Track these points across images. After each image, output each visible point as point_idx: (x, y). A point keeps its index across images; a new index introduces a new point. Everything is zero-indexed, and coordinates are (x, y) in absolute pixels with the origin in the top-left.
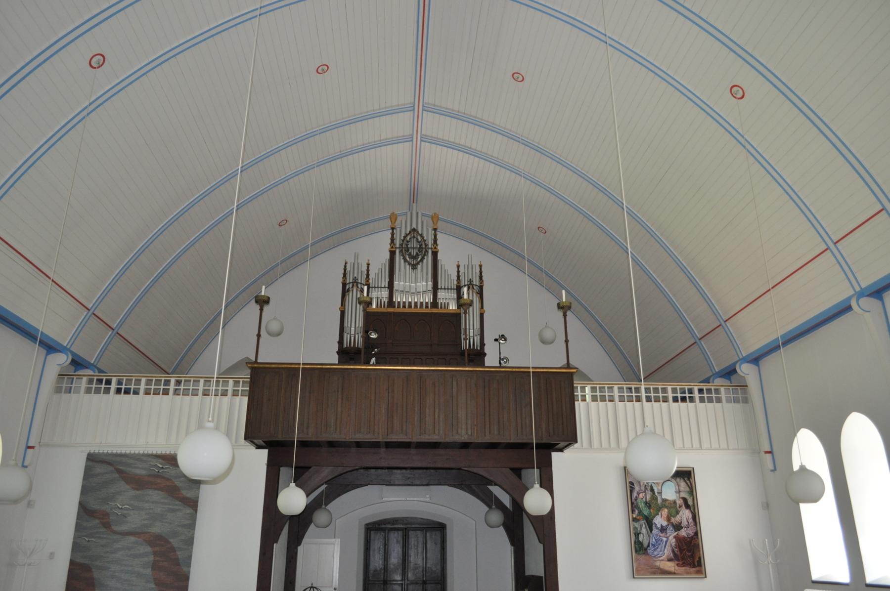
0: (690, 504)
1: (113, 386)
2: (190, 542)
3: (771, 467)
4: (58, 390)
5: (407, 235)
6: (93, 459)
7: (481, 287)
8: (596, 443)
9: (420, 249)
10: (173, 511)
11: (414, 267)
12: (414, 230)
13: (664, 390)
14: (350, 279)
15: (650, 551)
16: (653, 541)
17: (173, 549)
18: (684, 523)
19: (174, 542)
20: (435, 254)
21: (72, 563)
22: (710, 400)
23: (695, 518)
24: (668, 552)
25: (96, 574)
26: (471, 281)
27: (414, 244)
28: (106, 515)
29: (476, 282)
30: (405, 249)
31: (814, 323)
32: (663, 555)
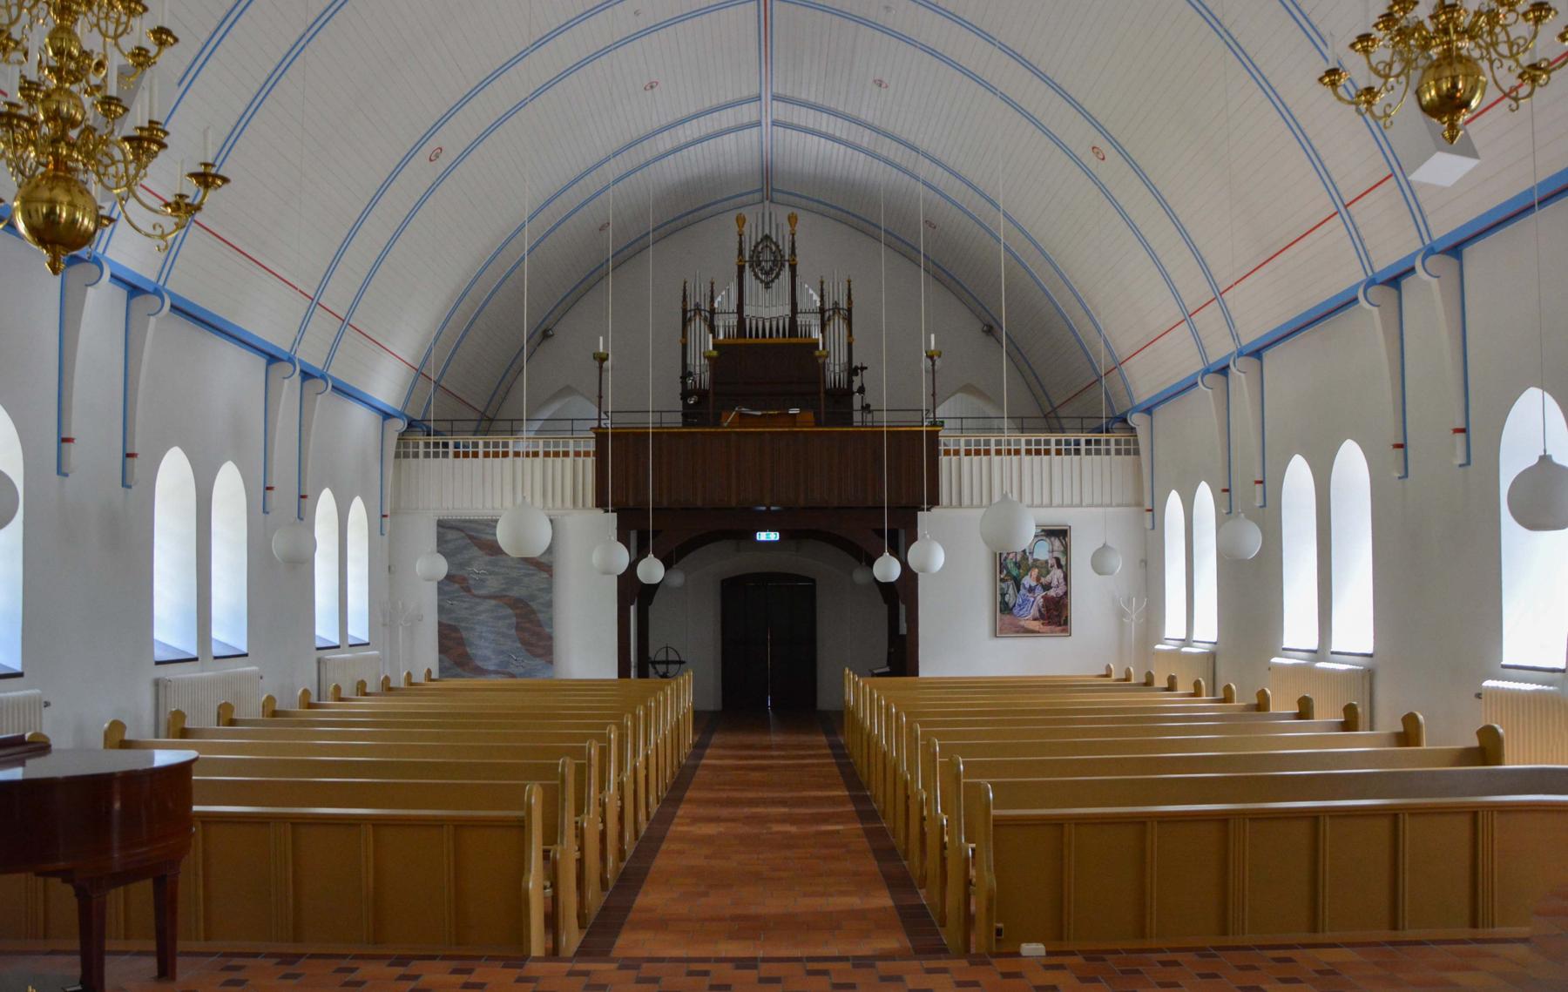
0: (1063, 565)
1: (451, 450)
2: (549, 604)
3: (1461, 459)
4: (397, 456)
6: (442, 525)
7: (849, 310)
8: (966, 500)
9: (775, 262)
10: (526, 575)
11: (767, 285)
12: (767, 238)
13: (1047, 442)
14: (691, 306)
15: (1015, 611)
16: (1020, 601)
17: (533, 612)
18: (1055, 583)
19: (534, 605)
20: (793, 268)
21: (440, 624)
22: (1098, 452)
23: (1066, 578)
24: (1034, 611)
25: (464, 634)
26: (836, 303)
27: (767, 255)
28: (464, 579)
29: (843, 304)
30: (756, 263)
31: (1325, 311)
32: (1028, 617)
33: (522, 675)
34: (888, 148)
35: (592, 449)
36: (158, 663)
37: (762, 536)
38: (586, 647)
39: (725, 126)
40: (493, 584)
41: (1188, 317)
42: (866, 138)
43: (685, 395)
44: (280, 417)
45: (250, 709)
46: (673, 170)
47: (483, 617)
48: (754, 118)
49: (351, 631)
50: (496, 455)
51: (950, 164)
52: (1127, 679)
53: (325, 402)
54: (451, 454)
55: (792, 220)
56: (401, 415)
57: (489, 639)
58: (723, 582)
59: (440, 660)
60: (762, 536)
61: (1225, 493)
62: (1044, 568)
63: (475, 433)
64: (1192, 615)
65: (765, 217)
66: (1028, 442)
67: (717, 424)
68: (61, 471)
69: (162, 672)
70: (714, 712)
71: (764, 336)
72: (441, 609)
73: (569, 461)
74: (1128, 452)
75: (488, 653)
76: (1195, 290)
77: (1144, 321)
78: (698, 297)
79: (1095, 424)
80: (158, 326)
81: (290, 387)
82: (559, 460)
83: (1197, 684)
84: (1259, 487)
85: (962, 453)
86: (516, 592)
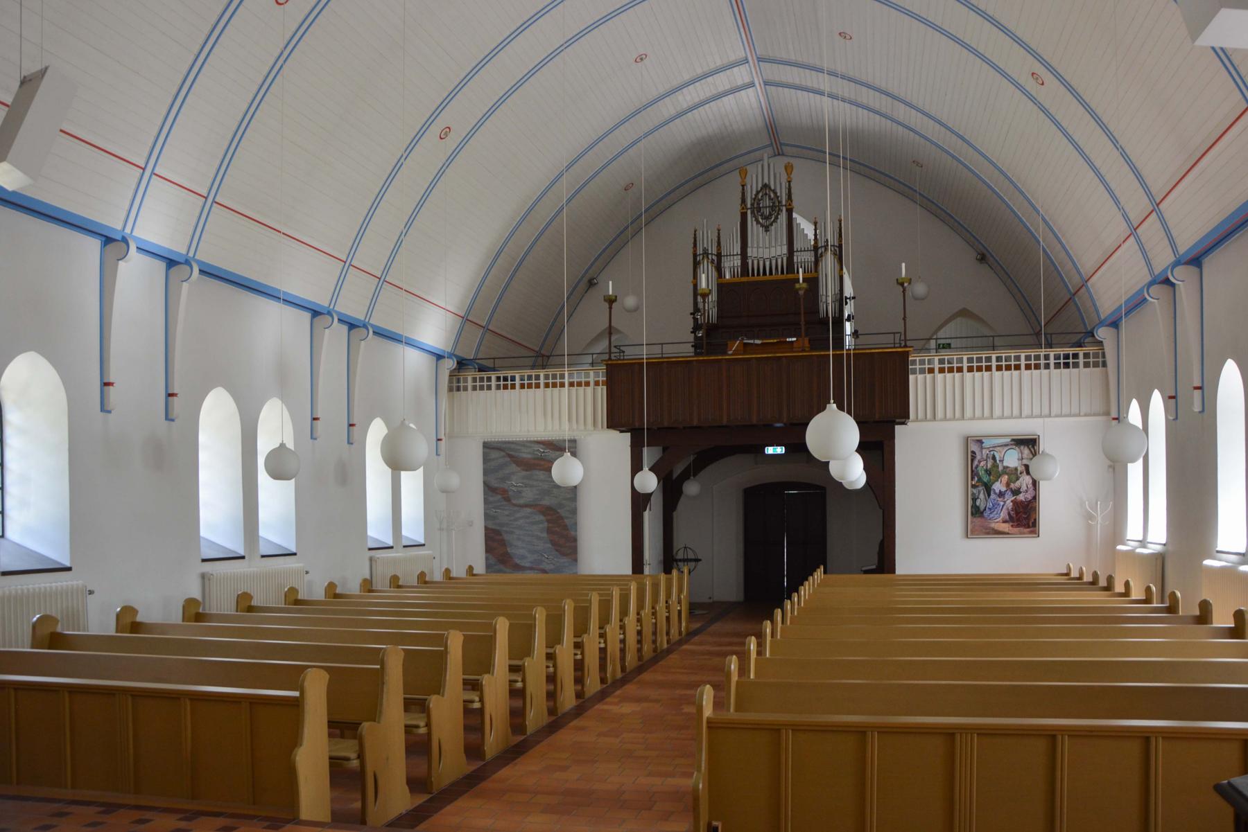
2: (574, 512)
4: (450, 389)
5: (758, 192)
6: (487, 446)
8: (940, 414)
9: (772, 208)
11: (767, 229)
12: (765, 186)
14: (700, 251)
15: (985, 515)
17: (561, 518)
18: (1024, 488)
19: (562, 512)
21: (486, 528)
24: (1004, 514)
25: (506, 537)
28: (504, 491)
30: (757, 209)
32: (998, 519)
33: (552, 571)
34: (866, 96)
35: (602, 378)
36: (204, 560)
37: (770, 450)
38: (605, 546)
39: (721, 89)
40: (529, 495)
41: (1134, 230)
42: (845, 89)
43: (696, 328)
44: (360, 359)
45: (223, 603)
46: (684, 133)
47: (520, 522)
48: (747, 80)
49: (405, 532)
50: (554, 385)
51: (920, 106)
52: (1080, 578)
53: (369, 345)
54: (518, 386)
55: (789, 168)
56: (451, 355)
57: (528, 539)
58: (824, 489)
59: (487, 559)
60: (770, 450)
61: (1171, 399)
62: (1014, 474)
63: (533, 367)
64: (1148, 524)
65: (749, 169)
66: (970, 360)
67: (725, 353)
68: (104, 408)
69: (208, 567)
70: (734, 603)
71: (771, 273)
72: (487, 516)
73: (589, 390)
74: (1096, 365)
75: (522, 552)
76: (1137, 205)
77: (1101, 240)
78: (707, 241)
79: (1075, 338)
80: (190, 288)
81: (334, 336)
82: (581, 389)
83: (1148, 589)
84: (1197, 393)
85: (936, 370)
86: (546, 502)
